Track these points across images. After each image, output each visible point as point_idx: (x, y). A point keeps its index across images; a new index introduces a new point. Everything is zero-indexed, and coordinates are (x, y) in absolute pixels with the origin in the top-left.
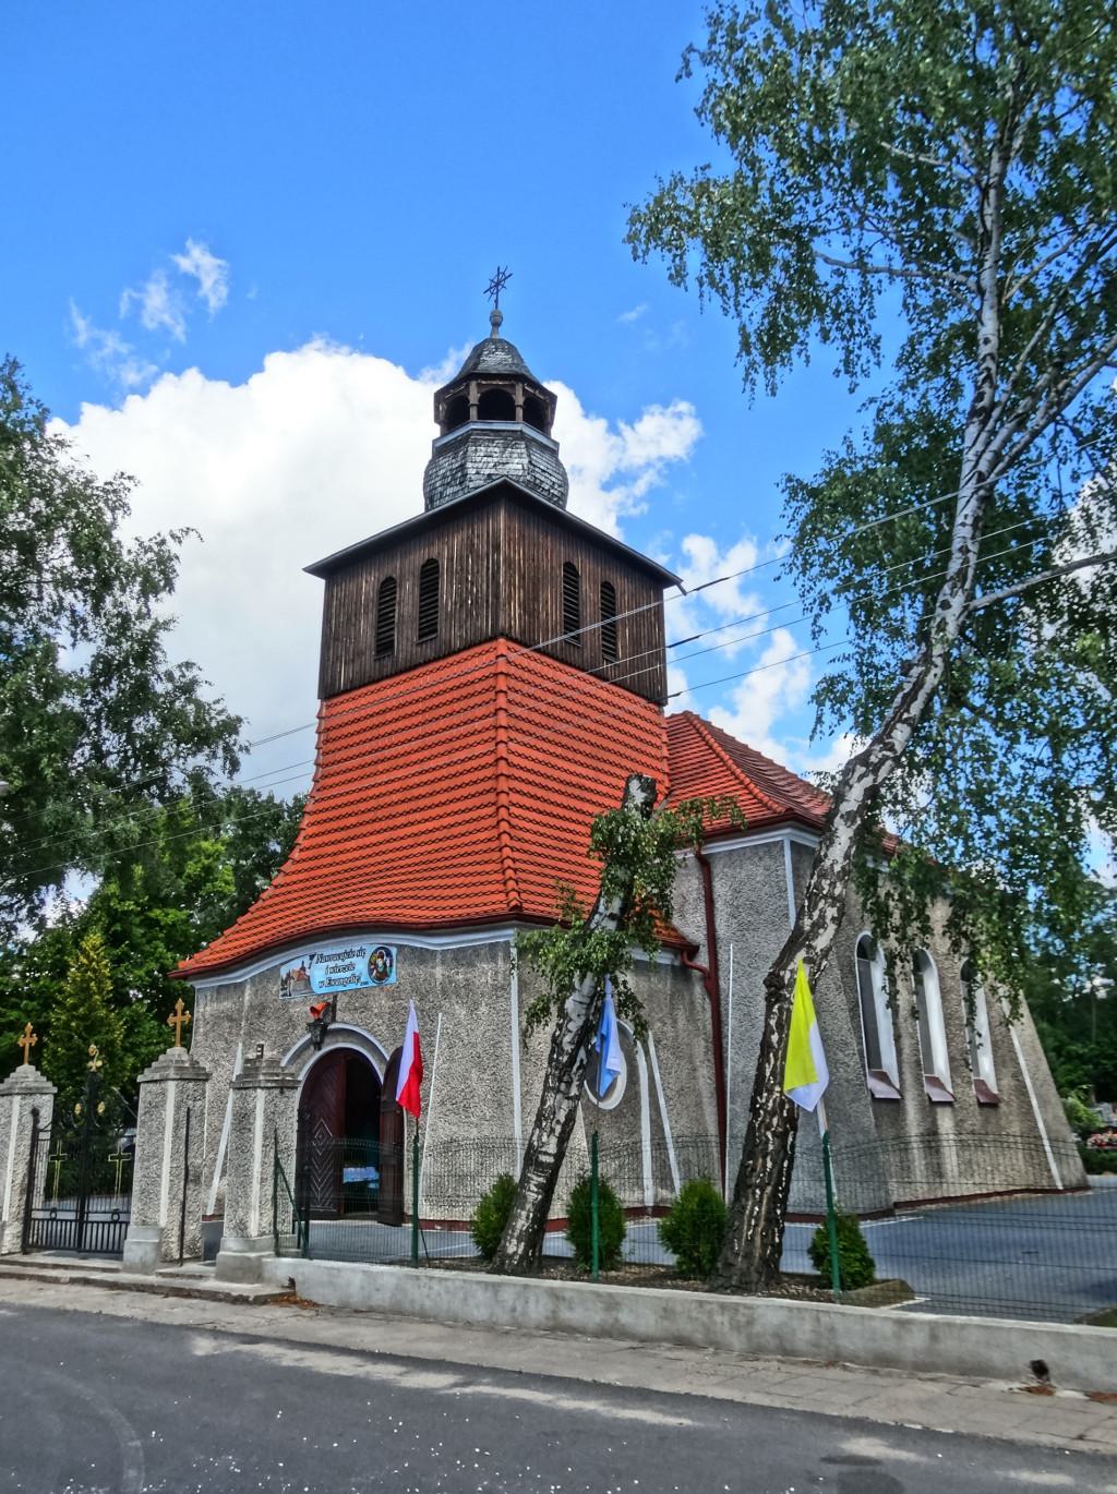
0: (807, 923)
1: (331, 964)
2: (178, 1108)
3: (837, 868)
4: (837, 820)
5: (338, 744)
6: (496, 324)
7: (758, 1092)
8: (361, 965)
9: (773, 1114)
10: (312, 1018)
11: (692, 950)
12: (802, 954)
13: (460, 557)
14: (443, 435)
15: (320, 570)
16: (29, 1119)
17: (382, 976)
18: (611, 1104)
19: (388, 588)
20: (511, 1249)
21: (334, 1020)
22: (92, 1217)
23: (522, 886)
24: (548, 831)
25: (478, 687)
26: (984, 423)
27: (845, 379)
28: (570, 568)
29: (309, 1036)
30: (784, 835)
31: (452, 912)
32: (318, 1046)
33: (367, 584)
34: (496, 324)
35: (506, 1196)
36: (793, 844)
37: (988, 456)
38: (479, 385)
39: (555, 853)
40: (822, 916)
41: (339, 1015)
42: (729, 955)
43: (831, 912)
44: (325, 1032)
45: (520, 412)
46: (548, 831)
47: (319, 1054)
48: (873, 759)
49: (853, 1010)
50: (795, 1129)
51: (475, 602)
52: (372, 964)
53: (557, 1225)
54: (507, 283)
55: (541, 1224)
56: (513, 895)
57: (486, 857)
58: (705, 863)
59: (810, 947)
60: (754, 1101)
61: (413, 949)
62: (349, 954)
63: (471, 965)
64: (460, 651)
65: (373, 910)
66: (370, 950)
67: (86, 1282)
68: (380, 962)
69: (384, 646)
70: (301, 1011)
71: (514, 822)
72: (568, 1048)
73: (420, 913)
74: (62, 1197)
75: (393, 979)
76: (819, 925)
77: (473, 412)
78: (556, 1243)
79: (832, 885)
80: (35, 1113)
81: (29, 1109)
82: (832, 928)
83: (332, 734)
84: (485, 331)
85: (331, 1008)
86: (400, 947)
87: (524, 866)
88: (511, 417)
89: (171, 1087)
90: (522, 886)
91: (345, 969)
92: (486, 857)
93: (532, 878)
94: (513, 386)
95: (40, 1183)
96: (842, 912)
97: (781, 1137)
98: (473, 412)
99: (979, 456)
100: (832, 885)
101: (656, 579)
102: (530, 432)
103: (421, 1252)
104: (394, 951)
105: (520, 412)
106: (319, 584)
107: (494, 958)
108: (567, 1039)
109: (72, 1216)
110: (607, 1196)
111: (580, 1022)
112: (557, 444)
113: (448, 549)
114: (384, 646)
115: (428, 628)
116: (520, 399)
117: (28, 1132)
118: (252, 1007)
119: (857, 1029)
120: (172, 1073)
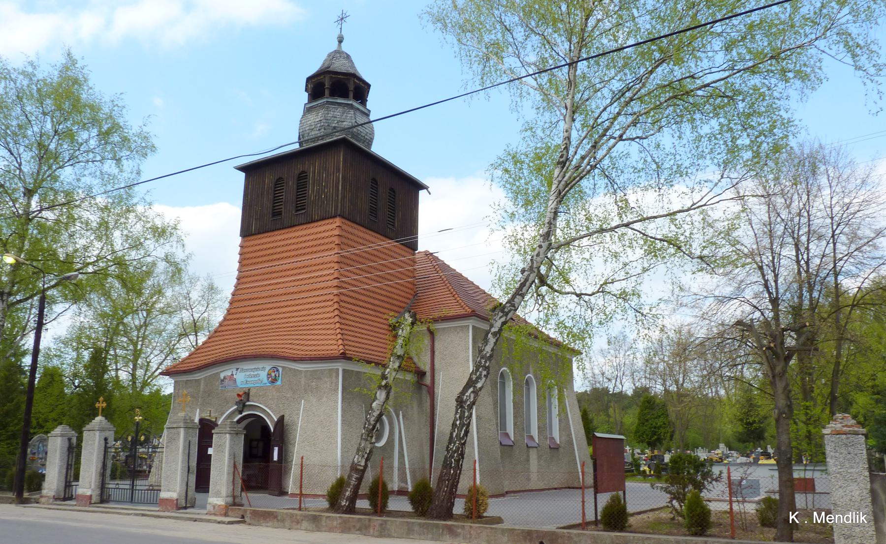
0: (474, 377)
1: (248, 373)
2: (185, 440)
3: (488, 355)
4: (490, 335)
5: (250, 261)
6: (340, 42)
7: (450, 443)
8: (263, 375)
9: (455, 452)
10: (238, 399)
11: (421, 374)
12: (471, 389)
13: (319, 173)
14: (310, 101)
15: (242, 169)
16: (103, 442)
17: (274, 381)
18: (381, 444)
19: (279, 182)
20: (343, 503)
21: (248, 401)
22: (138, 488)
23: (346, 342)
24: (358, 314)
25: (326, 241)
26: (563, 168)
27: (515, 114)
28: (374, 181)
29: (235, 407)
30: (470, 323)
31: (311, 353)
32: (241, 412)
33: (269, 179)
34: (340, 42)
35: (340, 484)
36: (473, 327)
37: (563, 183)
38: (331, 77)
39: (360, 325)
40: (480, 375)
41: (251, 398)
42: (440, 378)
43: (484, 373)
44: (244, 405)
45: (351, 95)
46: (358, 314)
47: (240, 416)
48: (506, 310)
49: (495, 404)
50: (463, 458)
51: (326, 197)
52: (269, 375)
53: (363, 497)
54: (347, 19)
55: (355, 496)
56: (341, 347)
57: (328, 326)
58: (432, 333)
59: (475, 387)
60: (448, 447)
61: (290, 369)
62: (257, 369)
63: (320, 379)
64: (317, 221)
65: (271, 349)
66: (268, 368)
67: (143, 515)
68: (273, 374)
69: (276, 213)
70: (233, 396)
71: (342, 310)
72: (373, 423)
73: (294, 352)
74: (121, 478)
75: (279, 383)
76: (479, 378)
77: (327, 92)
78: (363, 504)
79: (486, 362)
80: (106, 439)
81: (103, 438)
82: (484, 379)
83: (247, 256)
84: (334, 46)
85: (247, 394)
86: (283, 368)
87: (346, 332)
88: (345, 96)
89: (182, 431)
90: (346, 342)
91: (255, 376)
92: (328, 326)
93: (350, 338)
94: (349, 79)
95: (108, 472)
96: (488, 373)
97: (458, 461)
98: (327, 92)
99: (560, 182)
100: (486, 362)
101: (416, 186)
102: (356, 104)
103: (303, 506)
104: (280, 369)
105: (351, 95)
106: (242, 175)
107: (331, 376)
108: (373, 419)
109: (128, 487)
110: (384, 485)
111: (378, 412)
112: (369, 111)
113: (313, 168)
114: (276, 213)
115: (299, 208)
116: (351, 87)
117: (103, 448)
118: (205, 392)
119: (496, 413)
120: (182, 425)
